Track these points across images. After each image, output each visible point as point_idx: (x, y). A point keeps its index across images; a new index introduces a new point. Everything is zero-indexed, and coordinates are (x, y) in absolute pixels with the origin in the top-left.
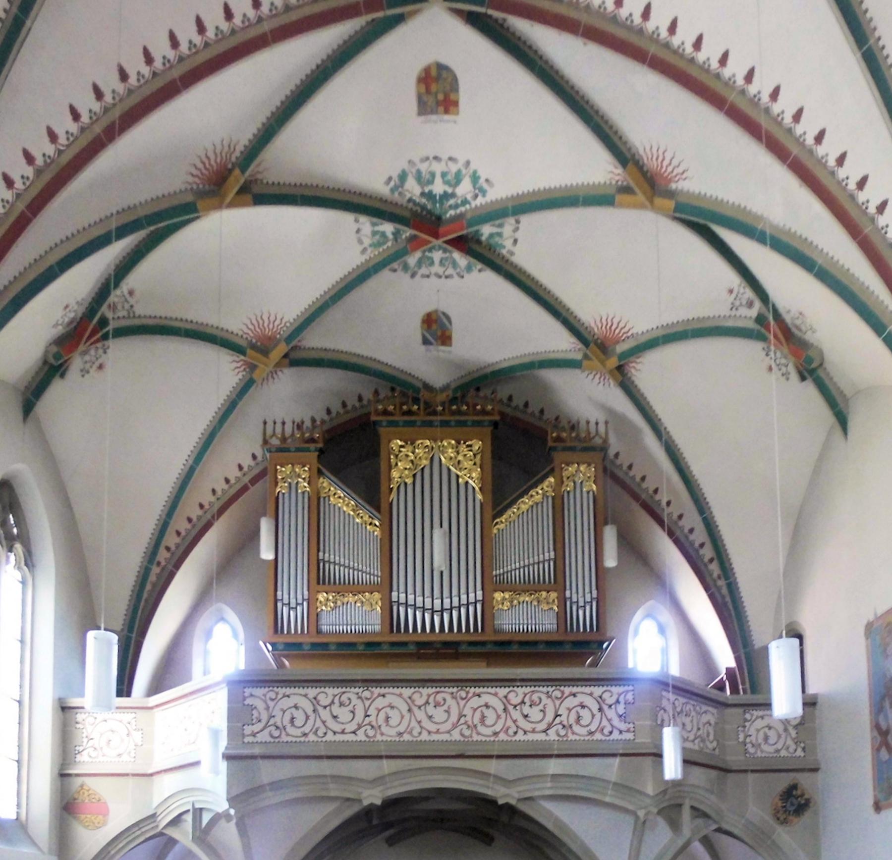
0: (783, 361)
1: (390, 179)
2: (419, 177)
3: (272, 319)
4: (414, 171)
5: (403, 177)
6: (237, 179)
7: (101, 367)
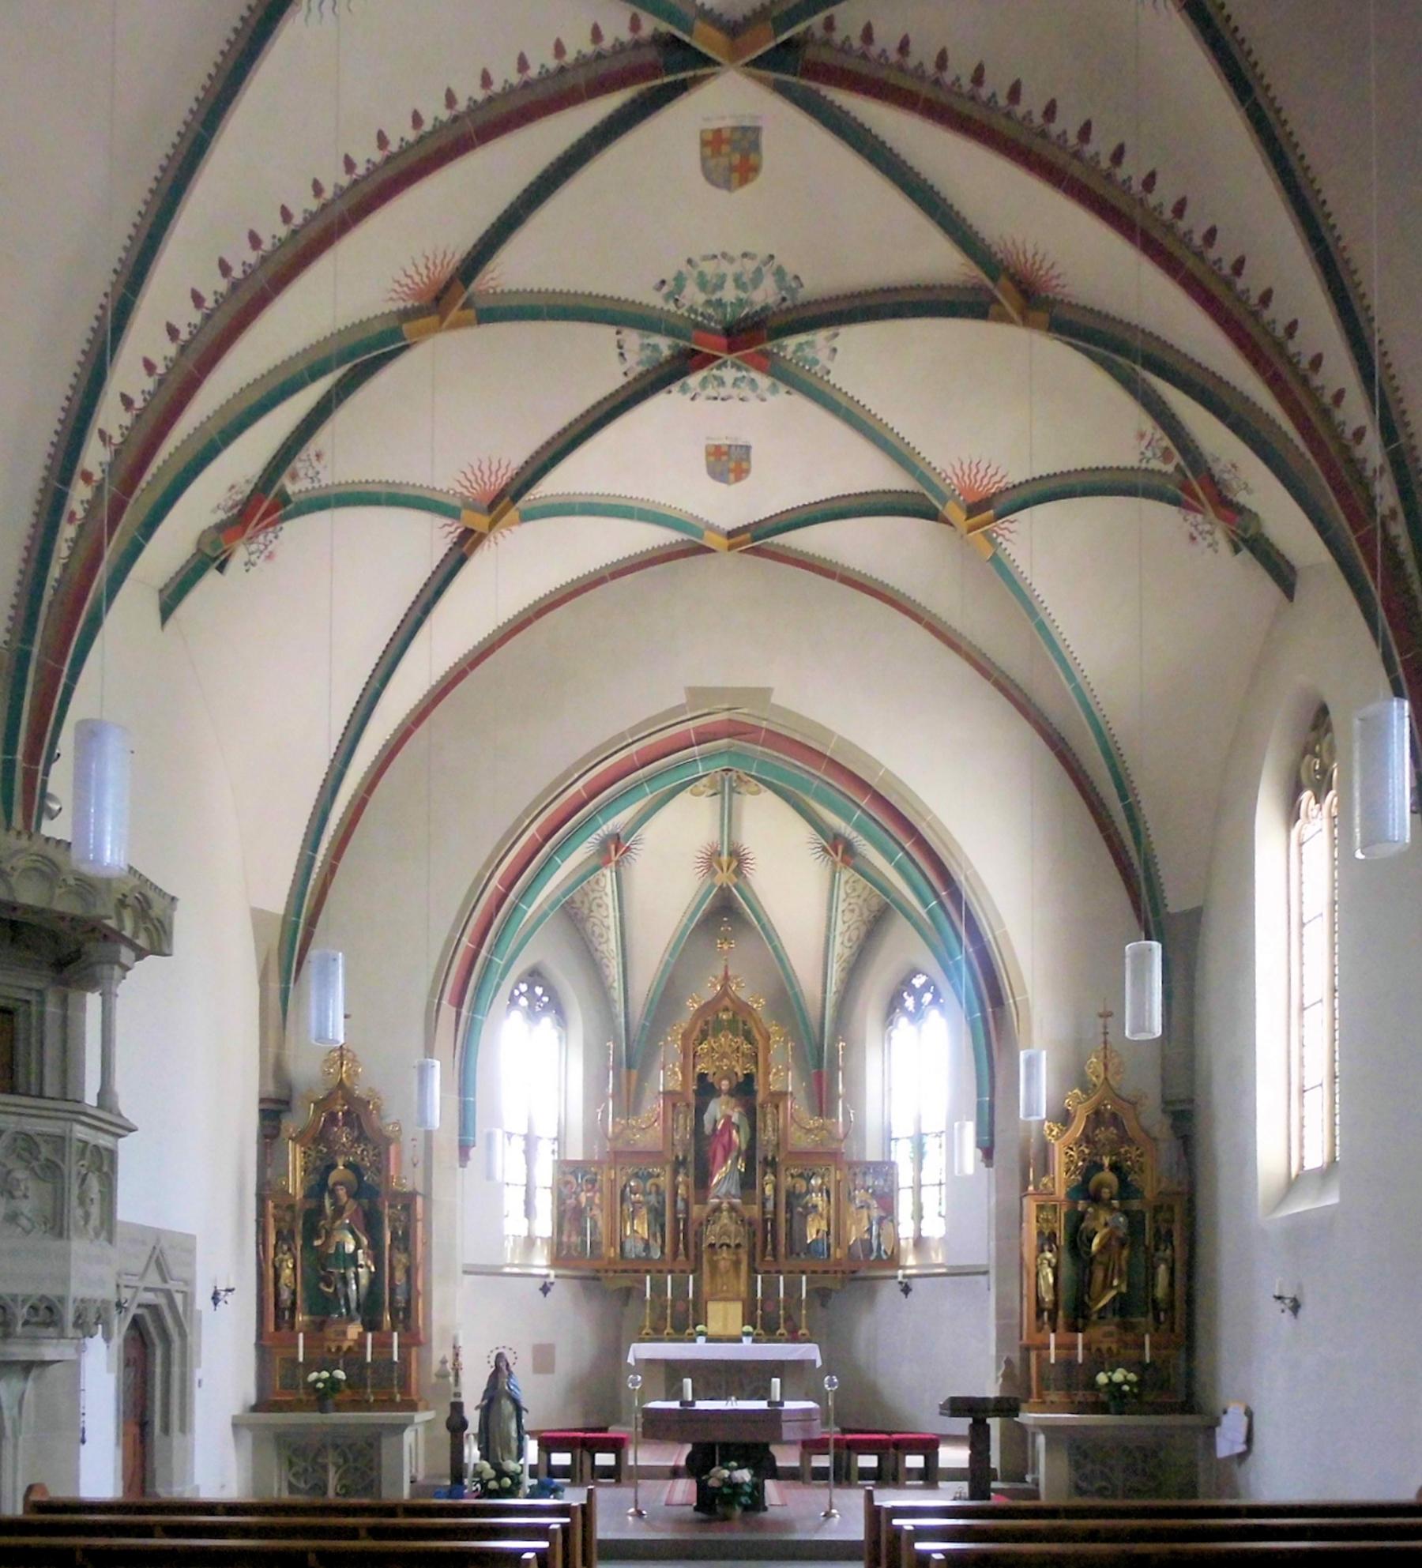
0: (1207, 527)
1: (663, 282)
2: (703, 284)
3: (494, 468)
4: (695, 274)
5: (680, 279)
6: (455, 295)
7: (270, 556)
